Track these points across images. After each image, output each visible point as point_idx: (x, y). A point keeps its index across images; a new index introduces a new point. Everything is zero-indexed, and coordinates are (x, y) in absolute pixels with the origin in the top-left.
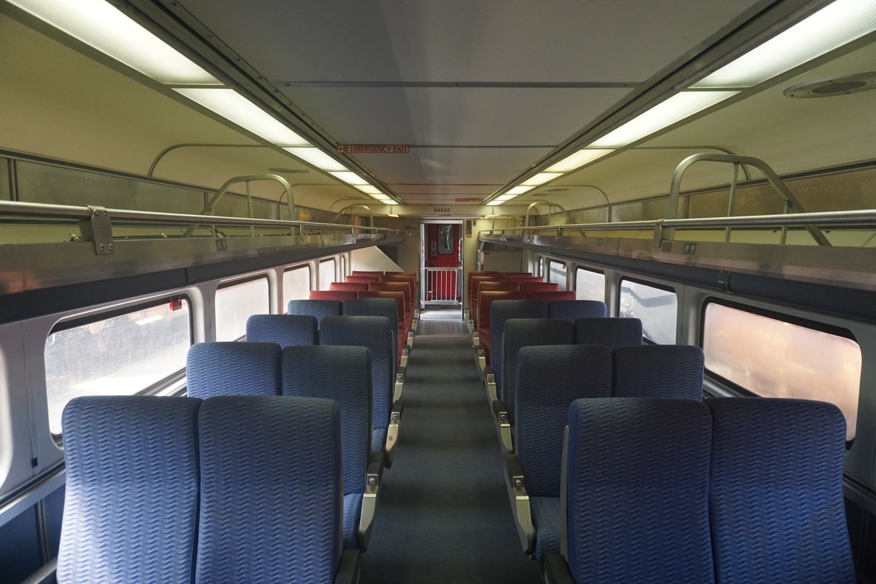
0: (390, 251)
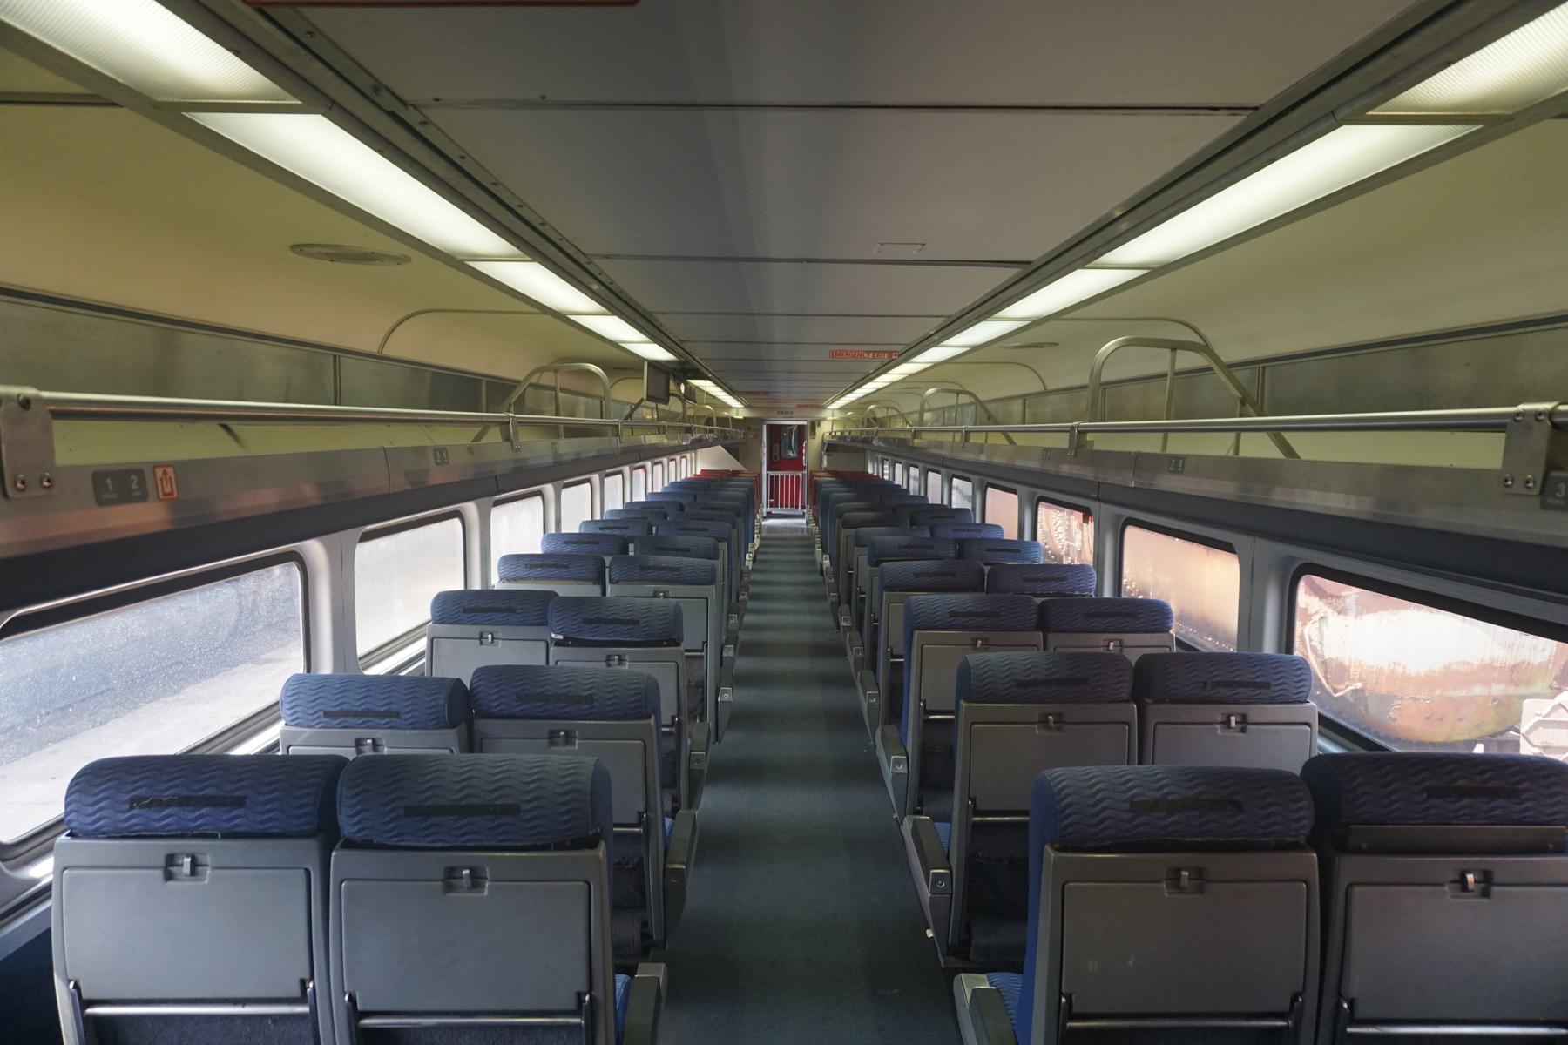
0: (733, 450)
